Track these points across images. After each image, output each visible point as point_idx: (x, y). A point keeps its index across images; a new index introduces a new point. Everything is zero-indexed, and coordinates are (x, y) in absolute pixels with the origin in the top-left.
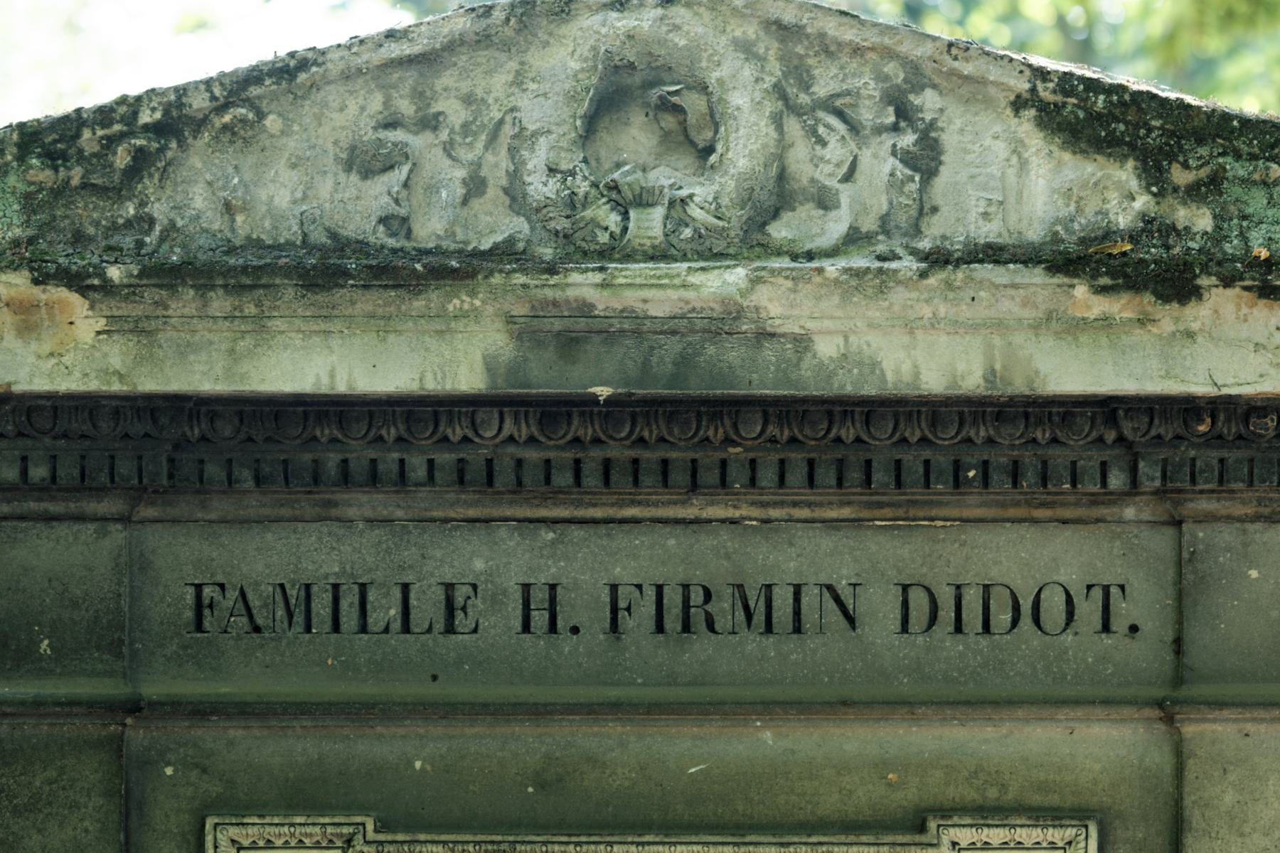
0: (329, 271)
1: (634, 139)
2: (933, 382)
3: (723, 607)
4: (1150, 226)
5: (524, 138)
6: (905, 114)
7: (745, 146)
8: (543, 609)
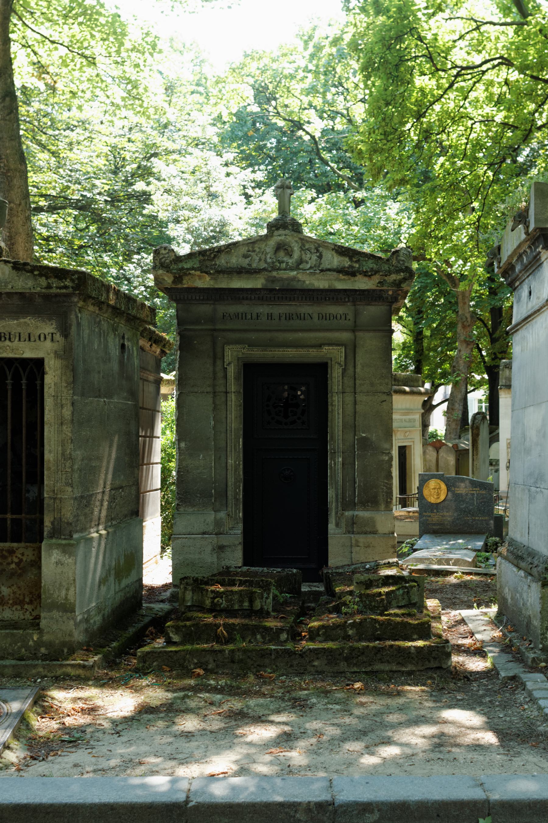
0: (240, 271)
1: (281, 254)
2: (321, 287)
3: (294, 316)
4: (351, 267)
5: (267, 254)
6: (318, 251)
7: (296, 255)
8: (270, 316)
